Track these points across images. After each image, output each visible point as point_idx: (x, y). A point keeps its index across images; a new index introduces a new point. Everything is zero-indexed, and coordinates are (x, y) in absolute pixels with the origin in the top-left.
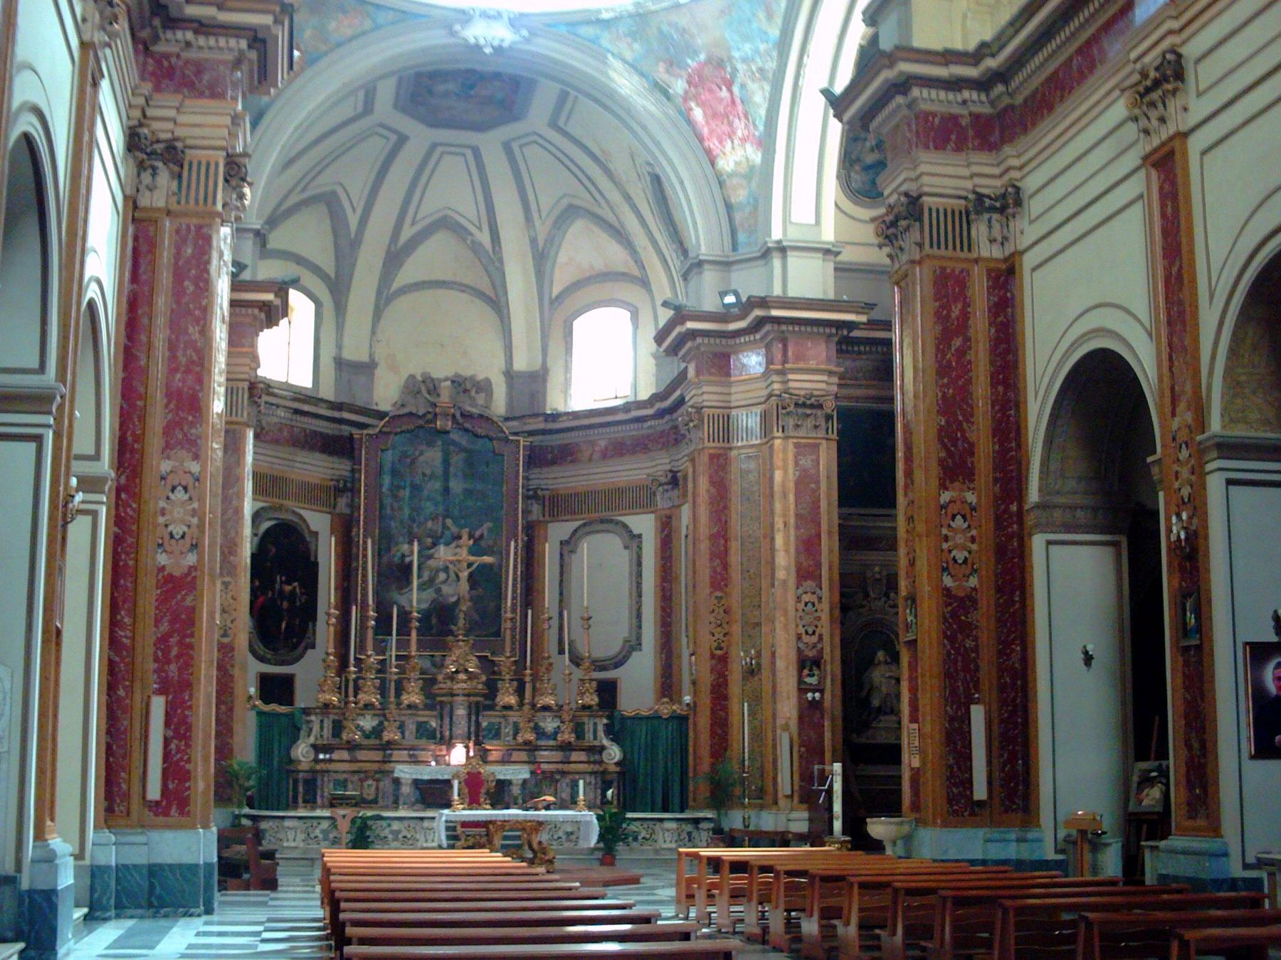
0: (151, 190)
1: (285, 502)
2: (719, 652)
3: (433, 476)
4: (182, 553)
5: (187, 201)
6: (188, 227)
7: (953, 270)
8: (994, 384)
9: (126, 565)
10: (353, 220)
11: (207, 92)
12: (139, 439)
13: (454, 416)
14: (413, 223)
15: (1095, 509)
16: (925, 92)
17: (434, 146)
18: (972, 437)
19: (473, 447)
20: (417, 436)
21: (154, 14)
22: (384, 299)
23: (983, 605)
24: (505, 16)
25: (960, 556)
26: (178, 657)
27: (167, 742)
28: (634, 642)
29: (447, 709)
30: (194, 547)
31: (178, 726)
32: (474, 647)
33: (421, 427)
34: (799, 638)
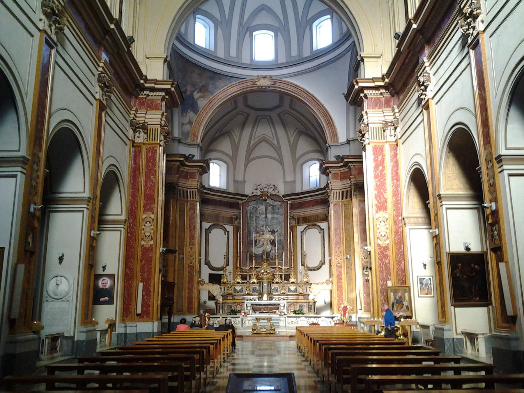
0: (139, 138)
1: (219, 223)
2: (339, 265)
3: (262, 214)
4: (149, 241)
5: (149, 140)
6: (150, 147)
7: (379, 146)
8: (393, 180)
9: (132, 245)
10: (275, 142)
11: (154, 108)
12: (136, 209)
13: (268, 195)
14: (254, 140)
16: (368, 91)
17: (258, 116)
18: (386, 196)
19: (273, 204)
20: (258, 202)
21: (136, 87)
22: (248, 161)
24: (268, 76)
26: (147, 271)
27: (143, 296)
28: (323, 261)
29: (261, 283)
30: (152, 239)
31: (147, 291)
32: (269, 265)
33: (258, 199)
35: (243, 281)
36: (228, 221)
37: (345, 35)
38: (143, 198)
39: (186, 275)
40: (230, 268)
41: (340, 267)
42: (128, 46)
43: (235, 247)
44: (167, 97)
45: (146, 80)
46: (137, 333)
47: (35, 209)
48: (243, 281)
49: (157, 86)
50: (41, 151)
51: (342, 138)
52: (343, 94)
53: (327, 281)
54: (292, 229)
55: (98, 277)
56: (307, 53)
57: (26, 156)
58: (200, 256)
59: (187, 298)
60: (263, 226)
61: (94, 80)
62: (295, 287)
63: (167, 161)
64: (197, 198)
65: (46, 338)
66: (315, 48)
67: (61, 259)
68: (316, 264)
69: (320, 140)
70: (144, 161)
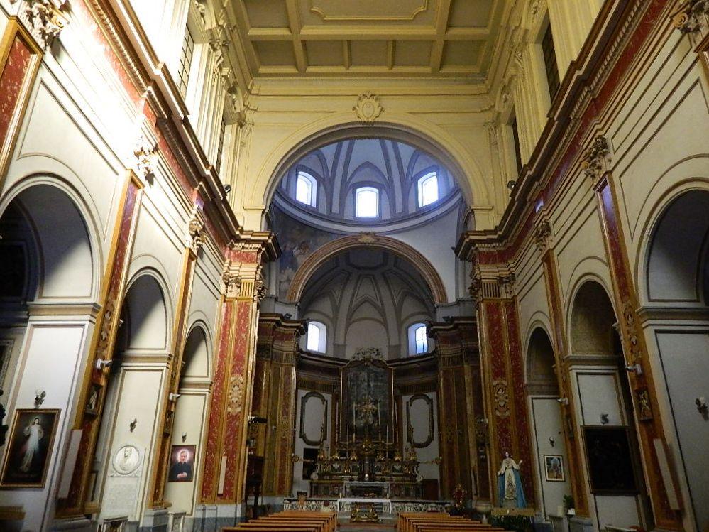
10: (379, 303)
15: (550, 386)
23: (512, 422)
25: (502, 404)
27: (226, 473)
34: (477, 435)
35: (342, 458)
36: (326, 388)
37: (454, 189)
38: (232, 358)
39: (278, 450)
40: (328, 443)
41: (452, 443)
42: (225, 195)
43: (334, 419)
44: (264, 249)
45: (242, 231)
46: (216, 519)
47: (102, 364)
48: (342, 458)
49: (253, 238)
50: (116, 298)
51: (451, 298)
52: (453, 248)
53: (436, 459)
54: (398, 399)
55: (177, 448)
56: (412, 210)
57: (97, 303)
58: (295, 427)
59: (278, 476)
60: (365, 395)
61: (186, 228)
62: (400, 467)
63: (260, 320)
64: (293, 361)
65: (105, 523)
66: (420, 205)
67: (133, 425)
68: (423, 440)
69: (427, 301)
70: (235, 318)
